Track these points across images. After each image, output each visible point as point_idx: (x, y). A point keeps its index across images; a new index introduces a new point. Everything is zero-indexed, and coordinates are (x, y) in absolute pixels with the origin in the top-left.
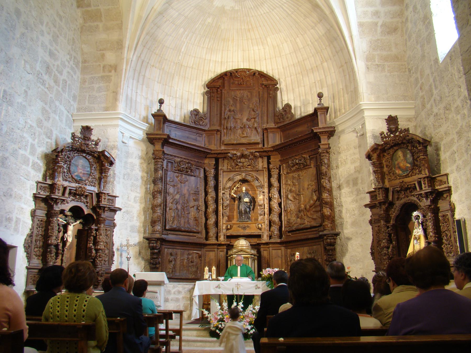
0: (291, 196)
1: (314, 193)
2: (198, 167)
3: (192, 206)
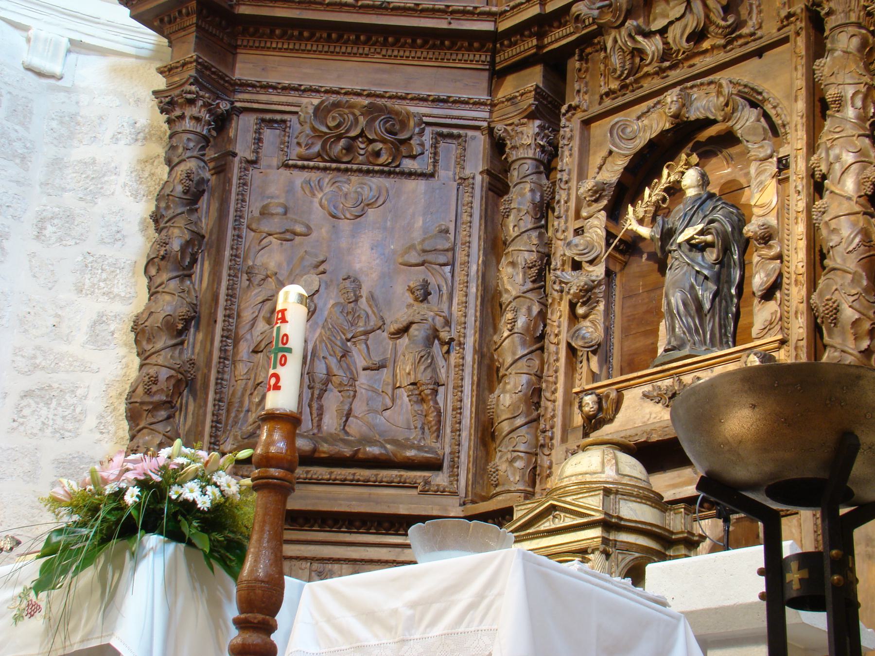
2: (445, 130)
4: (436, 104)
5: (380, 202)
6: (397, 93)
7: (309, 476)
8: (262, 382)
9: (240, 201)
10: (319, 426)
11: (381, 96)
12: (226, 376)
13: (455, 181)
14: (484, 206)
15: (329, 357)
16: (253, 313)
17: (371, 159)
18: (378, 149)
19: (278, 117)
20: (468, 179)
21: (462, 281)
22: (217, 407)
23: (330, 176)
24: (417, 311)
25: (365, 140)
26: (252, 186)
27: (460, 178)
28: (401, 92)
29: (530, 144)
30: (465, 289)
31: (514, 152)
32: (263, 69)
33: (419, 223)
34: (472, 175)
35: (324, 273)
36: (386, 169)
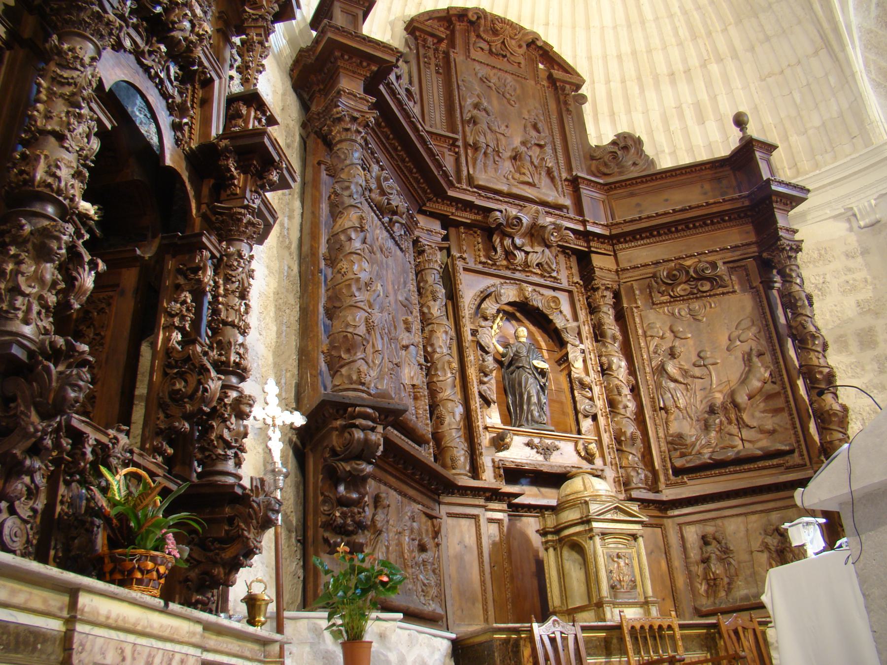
0: (674, 367)
1: (755, 359)
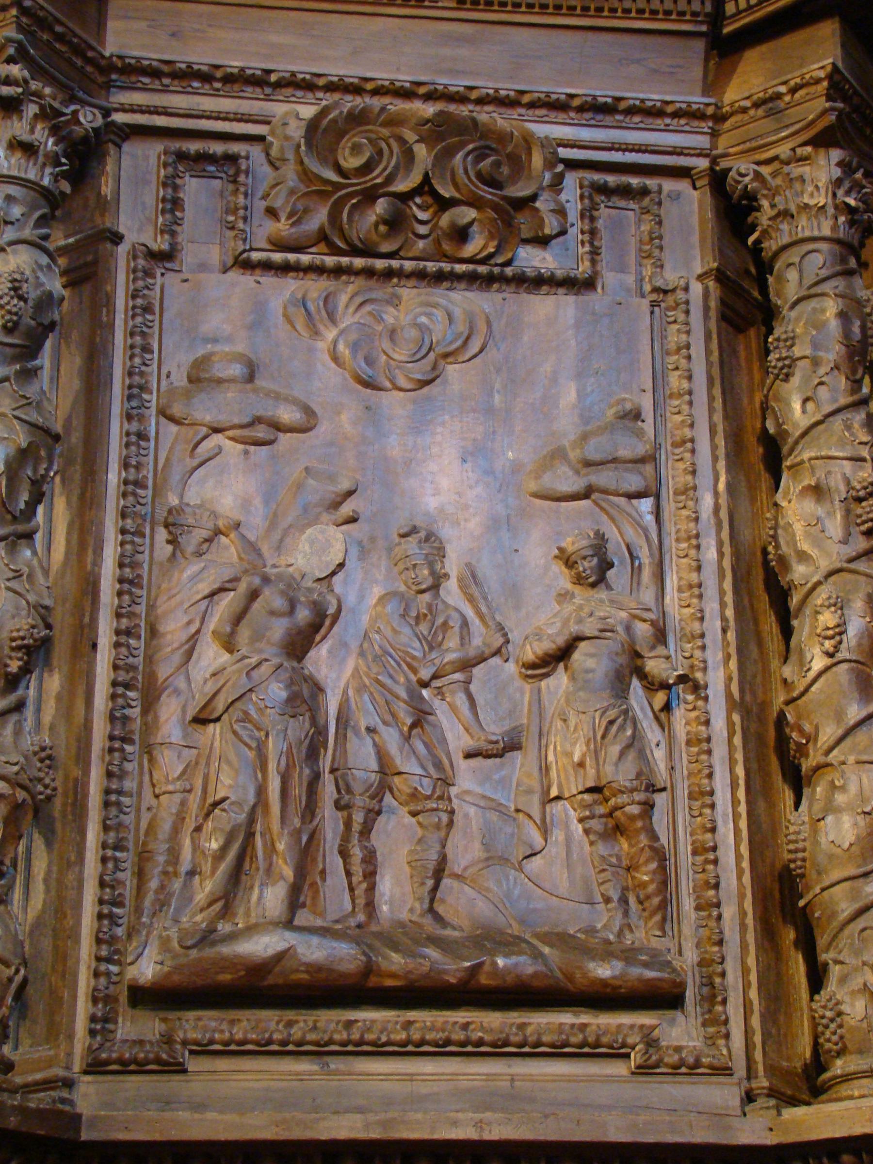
2: (611, 179)
3: (545, 646)
4: (589, 115)
5: (474, 347)
6: (497, 90)
7: (356, 1036)
8: (224, 800)
9: (137, 351)
10: (370, 906)
11: (460, 99)
12: (129, 784)
13: (643, 296)
14: (716, 354)
15: (381, 728)
16: (189, 623)
17: (447, 247)
18: (466, 220)
19: (217, 148)
20: (674, 290)
21: (683, 535)
22: (110, 865)
23: (351, 289)
24: (587, 610)
25: (429, 200)
26: (166, 316)
27: (656, 290)
28: (507, 87)
29: (823, 207)
30: (693, 552)
31: (785, 227)
32: (173, 35)
33: (569, 395)
34: (682, 283)
35: (353, 520)
36: (482, 269)
